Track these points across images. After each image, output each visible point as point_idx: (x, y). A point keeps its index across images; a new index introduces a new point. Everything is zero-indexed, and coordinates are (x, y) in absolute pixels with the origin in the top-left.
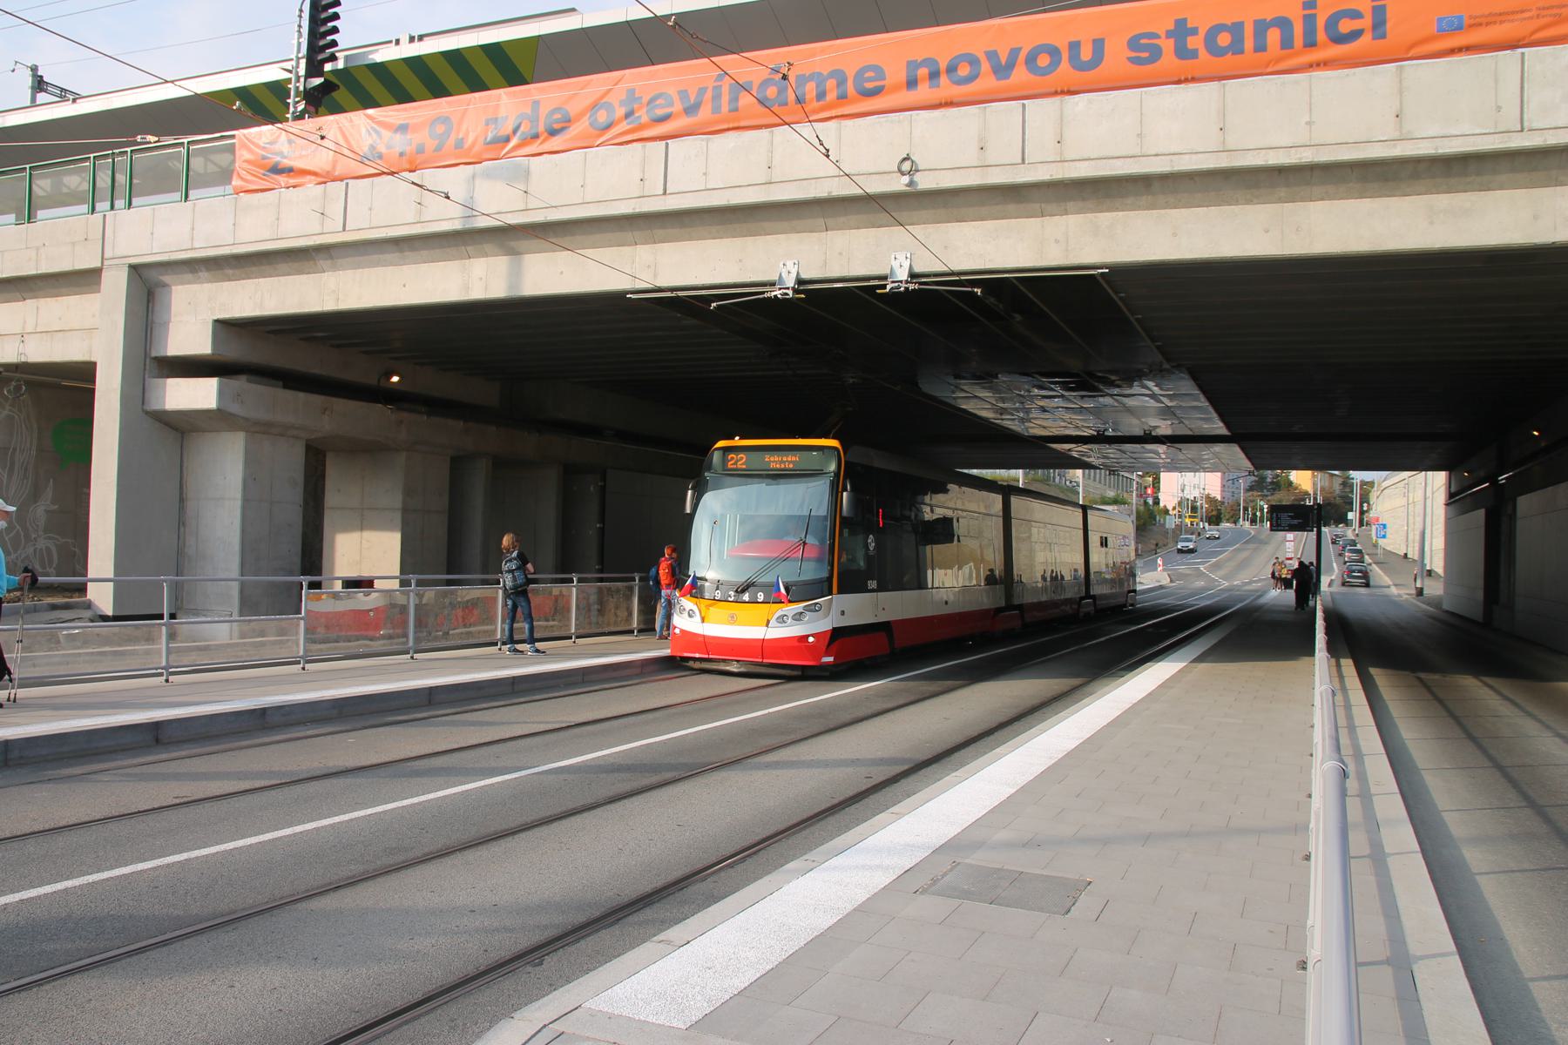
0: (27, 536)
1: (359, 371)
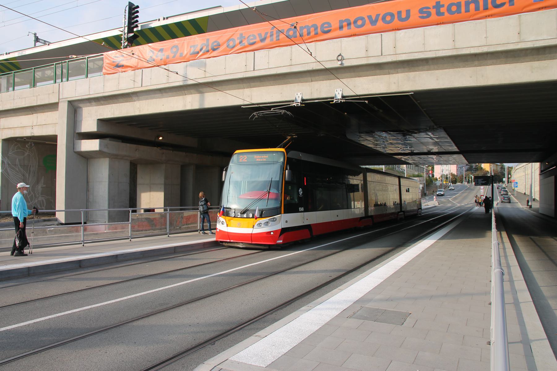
0: (35, 196)
1: (148, 136)
